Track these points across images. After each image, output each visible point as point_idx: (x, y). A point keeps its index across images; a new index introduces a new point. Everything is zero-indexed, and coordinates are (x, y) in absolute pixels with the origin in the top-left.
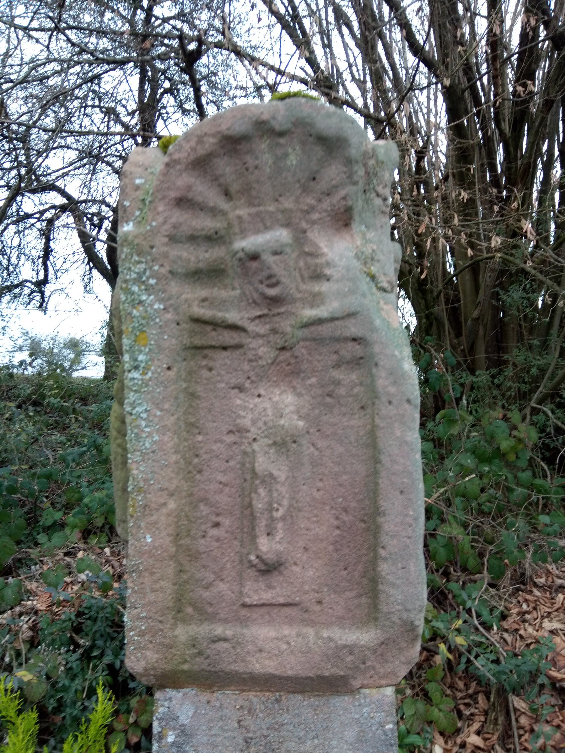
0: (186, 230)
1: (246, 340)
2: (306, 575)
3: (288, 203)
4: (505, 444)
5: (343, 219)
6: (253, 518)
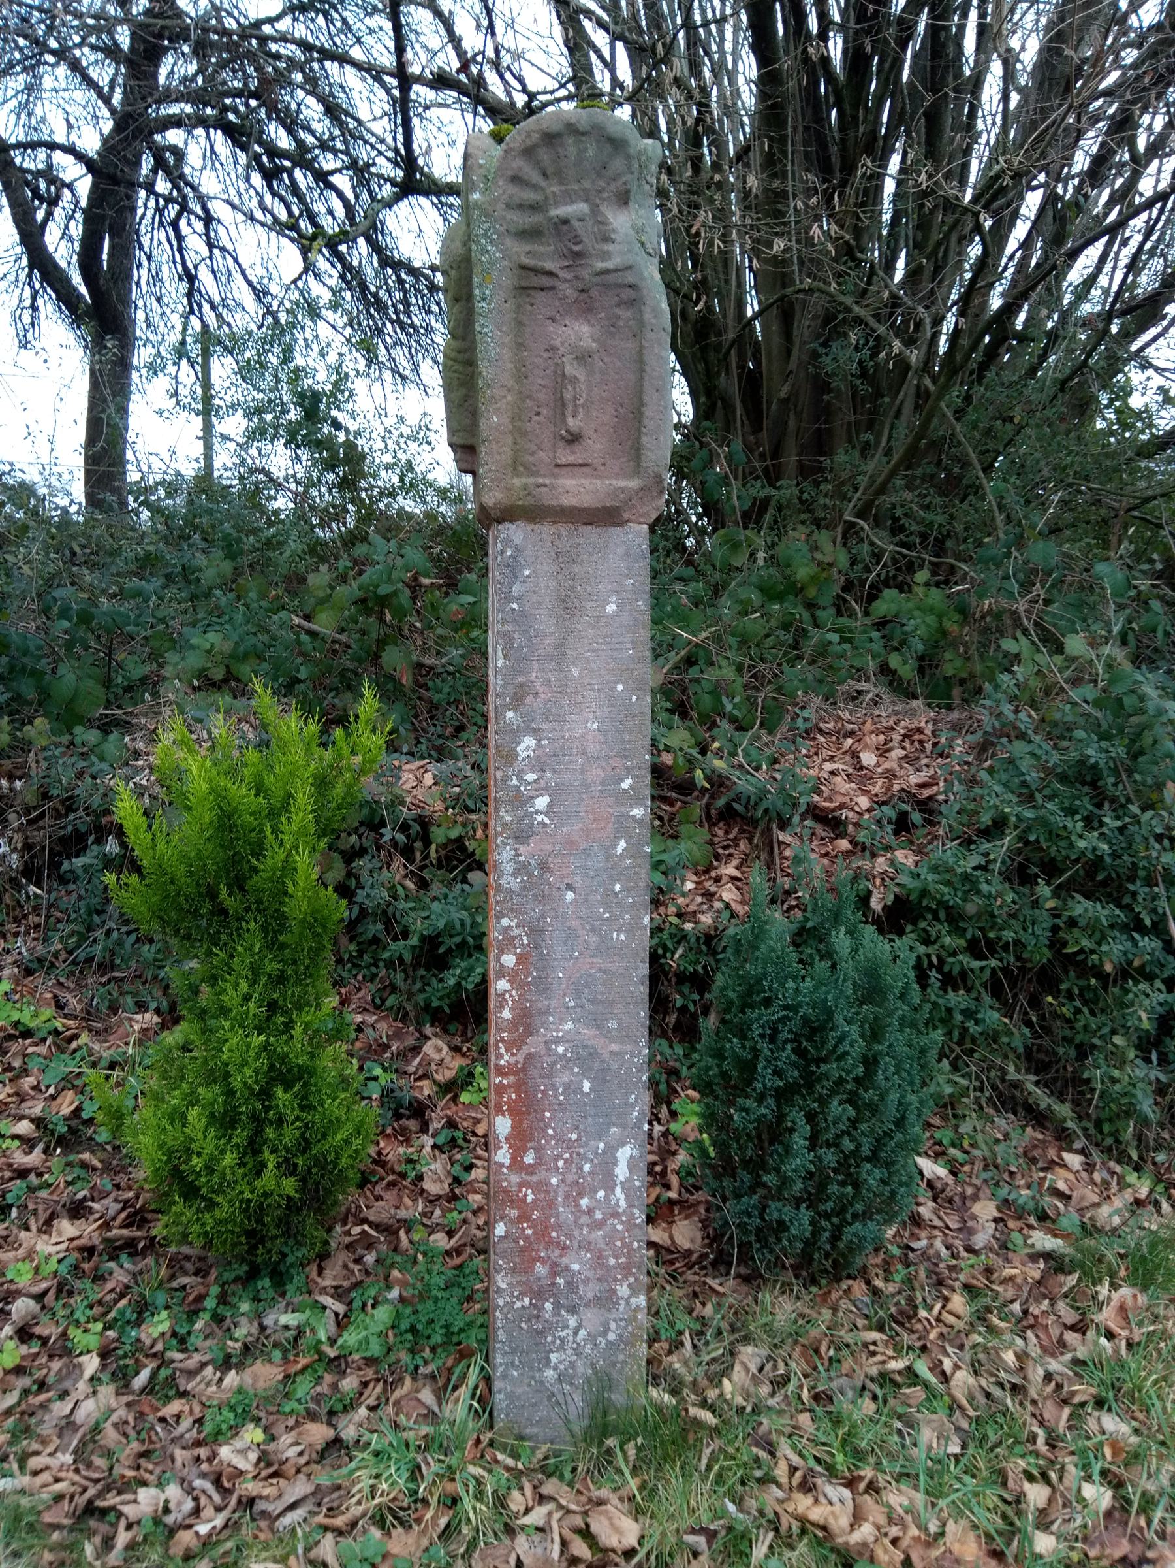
0: (516, 200)
1: (557, 283)
2: (595, 447)
3: (587, 184)
4: (803, 572)
5: (624, 199)
6: (564, 405)
